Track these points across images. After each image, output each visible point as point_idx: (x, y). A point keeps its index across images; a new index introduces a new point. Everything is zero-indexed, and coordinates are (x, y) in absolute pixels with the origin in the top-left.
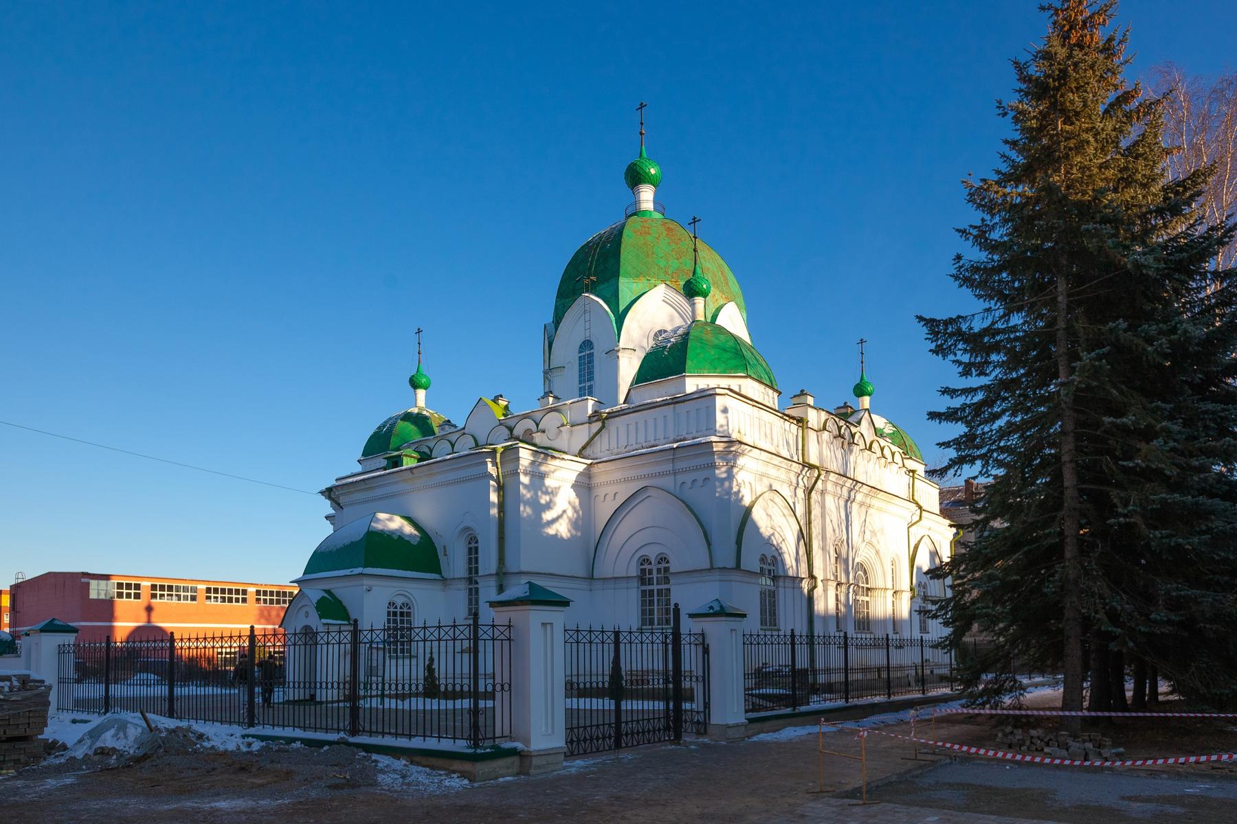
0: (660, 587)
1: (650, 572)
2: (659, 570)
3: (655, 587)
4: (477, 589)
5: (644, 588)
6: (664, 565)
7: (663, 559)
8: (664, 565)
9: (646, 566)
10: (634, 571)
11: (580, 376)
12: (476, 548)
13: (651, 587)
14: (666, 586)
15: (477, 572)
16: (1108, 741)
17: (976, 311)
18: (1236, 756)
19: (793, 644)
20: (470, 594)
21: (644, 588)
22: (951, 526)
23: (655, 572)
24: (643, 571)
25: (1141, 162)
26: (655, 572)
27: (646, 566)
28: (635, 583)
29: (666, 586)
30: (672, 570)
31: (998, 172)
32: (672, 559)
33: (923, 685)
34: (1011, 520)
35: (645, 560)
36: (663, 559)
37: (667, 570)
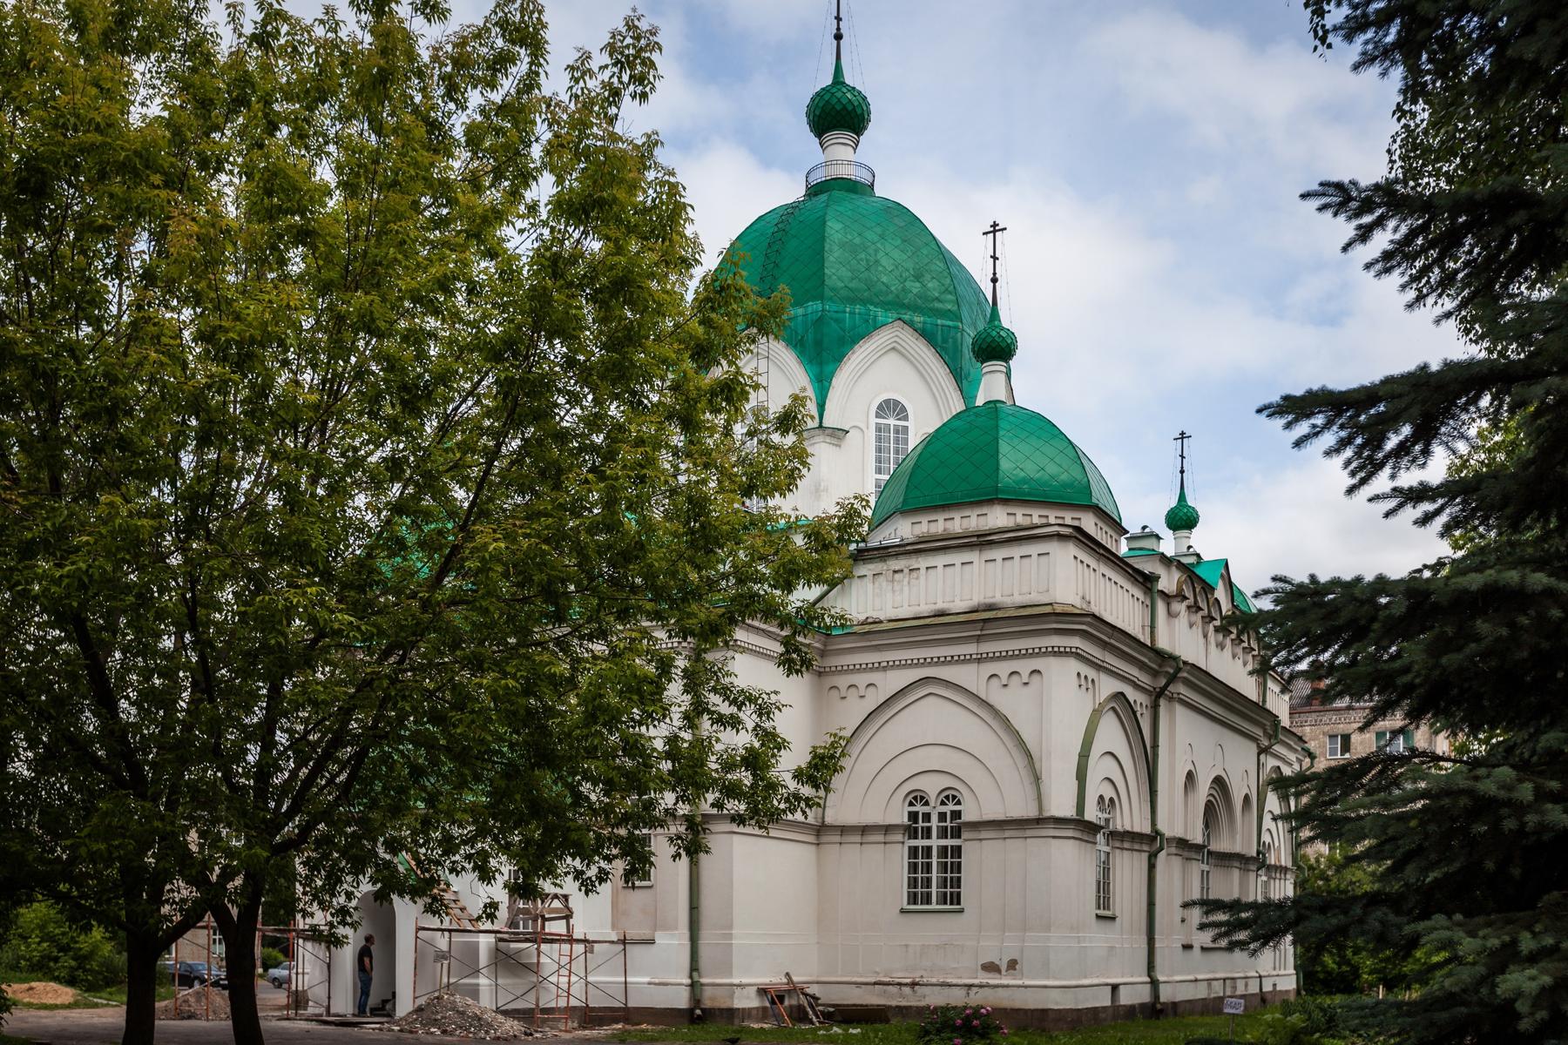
0: (926, 843)
1: (927, 817)
2: (942, 816)
3: (935, 842)
5: (914, 843)
6: (951, 807)
8: (951, 807)
9: (919, 808)
13: (943, 842)
14: (955, 842)
16: (356, 138)
17: (1421, 334)
22: (1335, 215)
23: (934, 818)
24: (913, 816)
26: (934, 818)
27: (919, 808)
29: (955, 842)
30: (965, 818)
31: (1403, 287)
32: (966, 796)
34: (275, 787)
35: (918, 797)
36: (950, 797)
37: (956, 815)
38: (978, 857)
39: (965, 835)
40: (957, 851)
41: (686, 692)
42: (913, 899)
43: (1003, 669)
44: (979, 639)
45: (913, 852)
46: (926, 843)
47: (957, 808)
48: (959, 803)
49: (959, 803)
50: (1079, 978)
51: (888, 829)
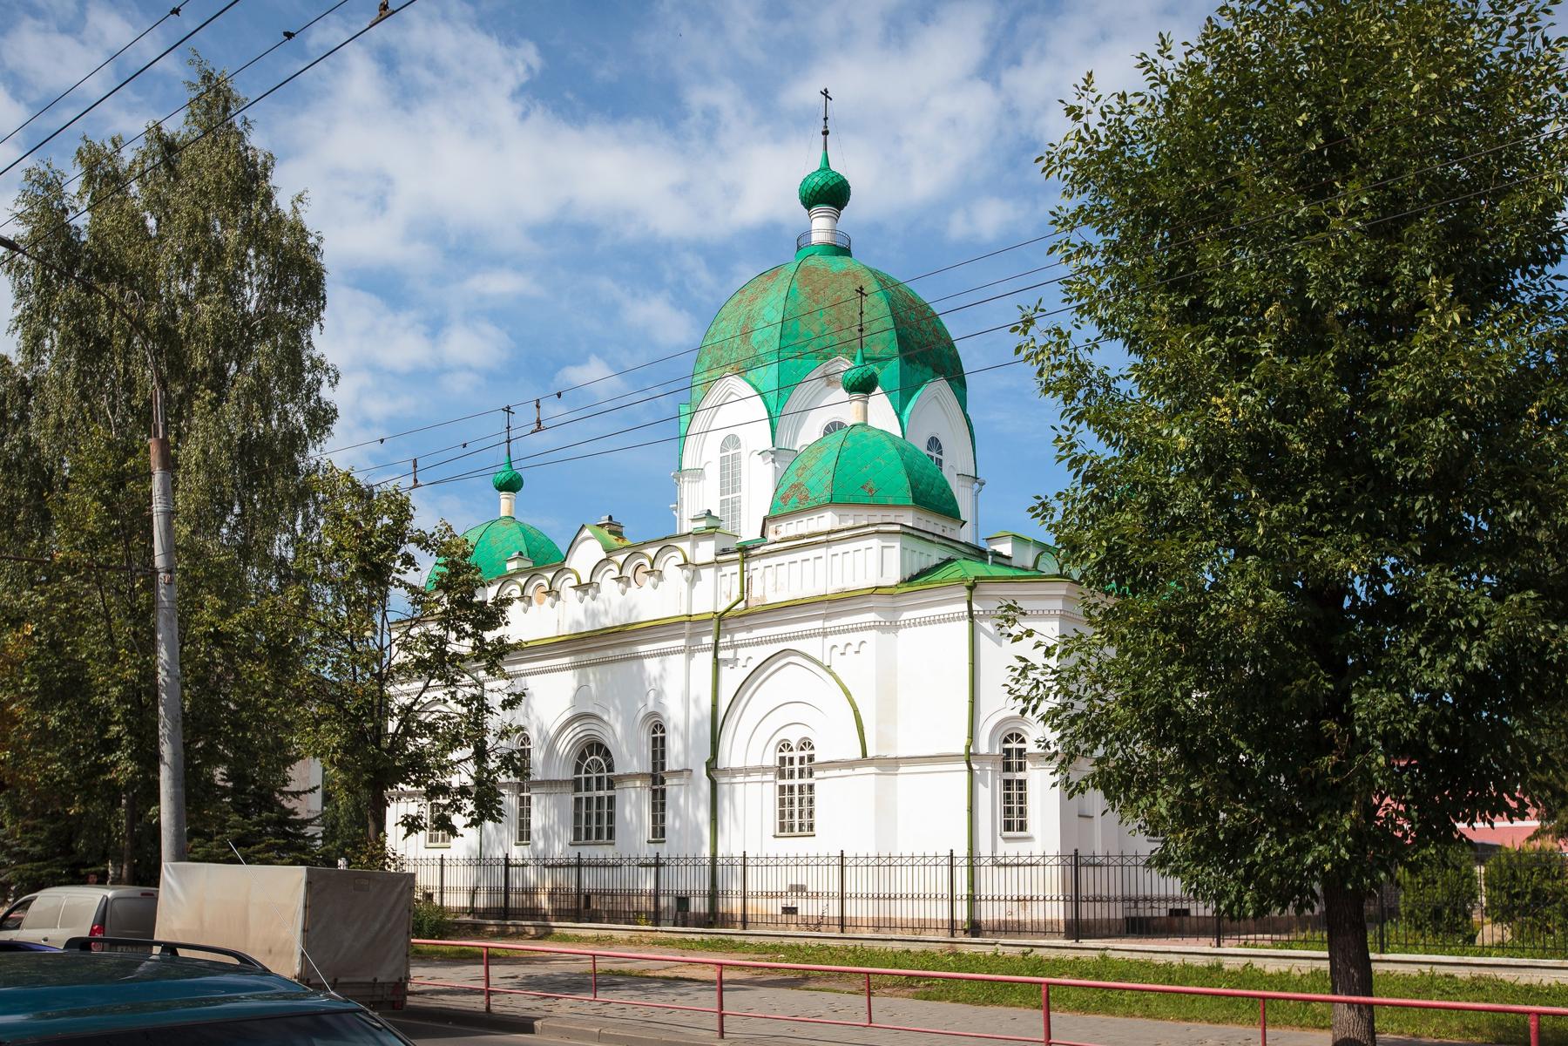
0: (802, 781)
1: (791, 760)
2: (802, 760)
4: (663, 791)
5: (783, 782)
6: (1014, 745)
7: (806, 744)
8: (805, 753)
9: (787, 754)
10: (771, 760)
11: (722, 484)
12: (663, 739)
15: (663, 768)
18: (1567, 849)
19: (442, 866)
20: (654, 797)
21: (783, 782)
23: (796, 761)
24: (782, 759)
25: (1241, 194)
26: (796, 761)
28: (770, 777)
30: (817, 759)
33: (842, 918)
35: (785, 745)
36: (806, 744)
38: (827, 789)
39: (816, 774)
40: (811, 787)
41: (413, 876)
42: (782, 828)
43: (840, 640)
44: (826, 617)
45: (782, 788)
46: (802, 781)
47: (1021, 746)
48: (1023, 741)
49: (1023, 741)
50: (1120, 980)
51: (763, 770)
